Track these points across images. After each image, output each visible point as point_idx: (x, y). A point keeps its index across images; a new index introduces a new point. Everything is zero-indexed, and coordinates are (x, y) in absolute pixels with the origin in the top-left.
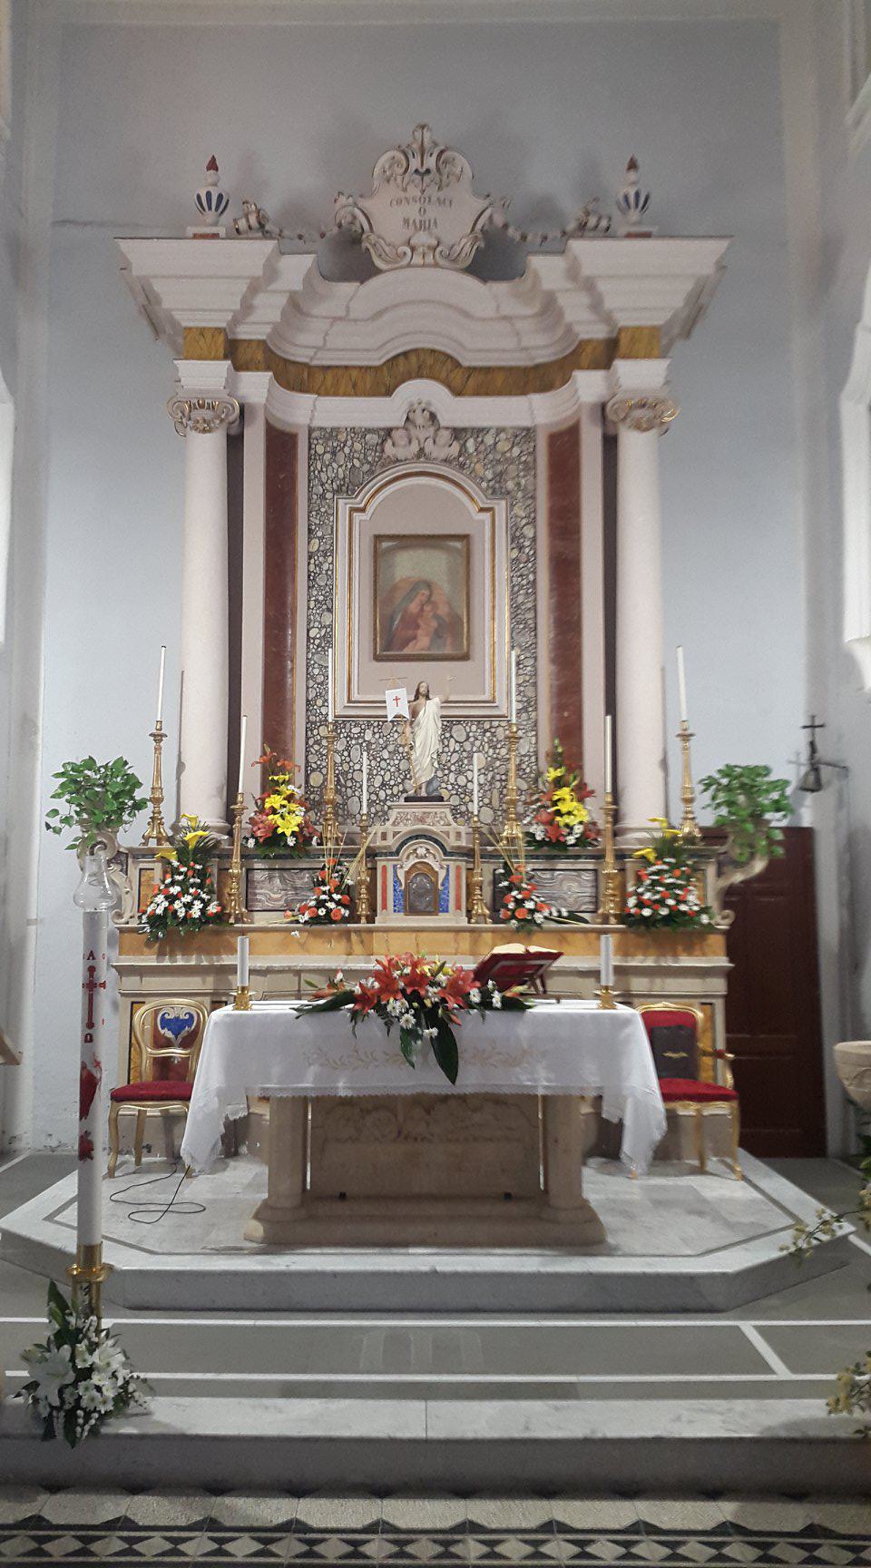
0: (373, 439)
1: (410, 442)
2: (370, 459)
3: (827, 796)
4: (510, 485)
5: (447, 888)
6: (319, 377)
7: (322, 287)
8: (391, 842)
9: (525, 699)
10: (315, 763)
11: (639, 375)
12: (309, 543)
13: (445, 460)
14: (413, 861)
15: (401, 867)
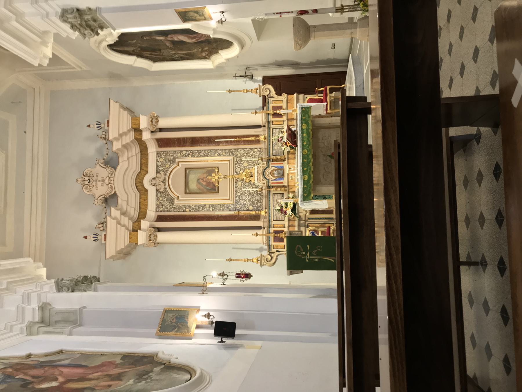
0: (159, 195)
1: (160, 185)
2: (164, 195)
3: (254, 73)
4: (172, 158)
5: (277, 166)
6: (142, 210)
7: (119, 207)
8: (265, 181)
9: (229, 152)
10: (246, 208)
11: (144, 123)
12: (187, 211)
13: (165, 175)
14: (270, 175)
15: (272, 178)
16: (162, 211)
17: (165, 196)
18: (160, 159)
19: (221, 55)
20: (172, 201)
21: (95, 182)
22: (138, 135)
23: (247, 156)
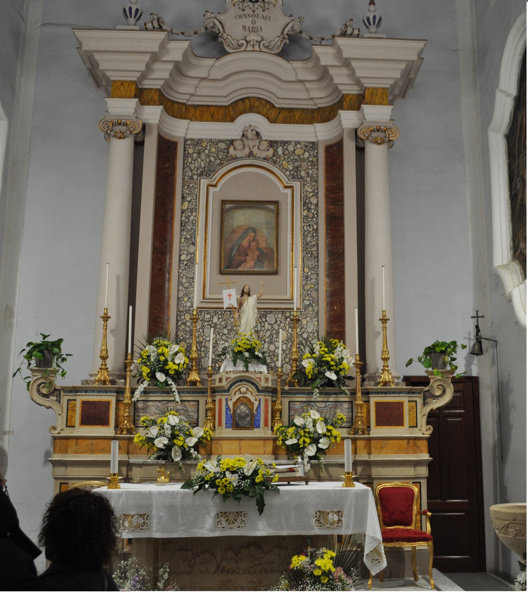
0: (222, 146)
1: (244, 148)
2: (220, 157)
3: (487, 357)
4: (303, 174)
5: (259, 413)
6: (192, 110)
8: (224, 383)
9: (311, 299)
13: (265, 159)
14: (238, 396)
15: (231, 400)
16: (186, 152)
17: (219, 159)
18: (301, 150)
19: (521, 284)
20: (208, 172)
21: (252, 13)
22: (350, 101)
23: (301, 339)
